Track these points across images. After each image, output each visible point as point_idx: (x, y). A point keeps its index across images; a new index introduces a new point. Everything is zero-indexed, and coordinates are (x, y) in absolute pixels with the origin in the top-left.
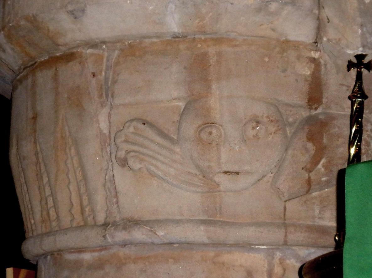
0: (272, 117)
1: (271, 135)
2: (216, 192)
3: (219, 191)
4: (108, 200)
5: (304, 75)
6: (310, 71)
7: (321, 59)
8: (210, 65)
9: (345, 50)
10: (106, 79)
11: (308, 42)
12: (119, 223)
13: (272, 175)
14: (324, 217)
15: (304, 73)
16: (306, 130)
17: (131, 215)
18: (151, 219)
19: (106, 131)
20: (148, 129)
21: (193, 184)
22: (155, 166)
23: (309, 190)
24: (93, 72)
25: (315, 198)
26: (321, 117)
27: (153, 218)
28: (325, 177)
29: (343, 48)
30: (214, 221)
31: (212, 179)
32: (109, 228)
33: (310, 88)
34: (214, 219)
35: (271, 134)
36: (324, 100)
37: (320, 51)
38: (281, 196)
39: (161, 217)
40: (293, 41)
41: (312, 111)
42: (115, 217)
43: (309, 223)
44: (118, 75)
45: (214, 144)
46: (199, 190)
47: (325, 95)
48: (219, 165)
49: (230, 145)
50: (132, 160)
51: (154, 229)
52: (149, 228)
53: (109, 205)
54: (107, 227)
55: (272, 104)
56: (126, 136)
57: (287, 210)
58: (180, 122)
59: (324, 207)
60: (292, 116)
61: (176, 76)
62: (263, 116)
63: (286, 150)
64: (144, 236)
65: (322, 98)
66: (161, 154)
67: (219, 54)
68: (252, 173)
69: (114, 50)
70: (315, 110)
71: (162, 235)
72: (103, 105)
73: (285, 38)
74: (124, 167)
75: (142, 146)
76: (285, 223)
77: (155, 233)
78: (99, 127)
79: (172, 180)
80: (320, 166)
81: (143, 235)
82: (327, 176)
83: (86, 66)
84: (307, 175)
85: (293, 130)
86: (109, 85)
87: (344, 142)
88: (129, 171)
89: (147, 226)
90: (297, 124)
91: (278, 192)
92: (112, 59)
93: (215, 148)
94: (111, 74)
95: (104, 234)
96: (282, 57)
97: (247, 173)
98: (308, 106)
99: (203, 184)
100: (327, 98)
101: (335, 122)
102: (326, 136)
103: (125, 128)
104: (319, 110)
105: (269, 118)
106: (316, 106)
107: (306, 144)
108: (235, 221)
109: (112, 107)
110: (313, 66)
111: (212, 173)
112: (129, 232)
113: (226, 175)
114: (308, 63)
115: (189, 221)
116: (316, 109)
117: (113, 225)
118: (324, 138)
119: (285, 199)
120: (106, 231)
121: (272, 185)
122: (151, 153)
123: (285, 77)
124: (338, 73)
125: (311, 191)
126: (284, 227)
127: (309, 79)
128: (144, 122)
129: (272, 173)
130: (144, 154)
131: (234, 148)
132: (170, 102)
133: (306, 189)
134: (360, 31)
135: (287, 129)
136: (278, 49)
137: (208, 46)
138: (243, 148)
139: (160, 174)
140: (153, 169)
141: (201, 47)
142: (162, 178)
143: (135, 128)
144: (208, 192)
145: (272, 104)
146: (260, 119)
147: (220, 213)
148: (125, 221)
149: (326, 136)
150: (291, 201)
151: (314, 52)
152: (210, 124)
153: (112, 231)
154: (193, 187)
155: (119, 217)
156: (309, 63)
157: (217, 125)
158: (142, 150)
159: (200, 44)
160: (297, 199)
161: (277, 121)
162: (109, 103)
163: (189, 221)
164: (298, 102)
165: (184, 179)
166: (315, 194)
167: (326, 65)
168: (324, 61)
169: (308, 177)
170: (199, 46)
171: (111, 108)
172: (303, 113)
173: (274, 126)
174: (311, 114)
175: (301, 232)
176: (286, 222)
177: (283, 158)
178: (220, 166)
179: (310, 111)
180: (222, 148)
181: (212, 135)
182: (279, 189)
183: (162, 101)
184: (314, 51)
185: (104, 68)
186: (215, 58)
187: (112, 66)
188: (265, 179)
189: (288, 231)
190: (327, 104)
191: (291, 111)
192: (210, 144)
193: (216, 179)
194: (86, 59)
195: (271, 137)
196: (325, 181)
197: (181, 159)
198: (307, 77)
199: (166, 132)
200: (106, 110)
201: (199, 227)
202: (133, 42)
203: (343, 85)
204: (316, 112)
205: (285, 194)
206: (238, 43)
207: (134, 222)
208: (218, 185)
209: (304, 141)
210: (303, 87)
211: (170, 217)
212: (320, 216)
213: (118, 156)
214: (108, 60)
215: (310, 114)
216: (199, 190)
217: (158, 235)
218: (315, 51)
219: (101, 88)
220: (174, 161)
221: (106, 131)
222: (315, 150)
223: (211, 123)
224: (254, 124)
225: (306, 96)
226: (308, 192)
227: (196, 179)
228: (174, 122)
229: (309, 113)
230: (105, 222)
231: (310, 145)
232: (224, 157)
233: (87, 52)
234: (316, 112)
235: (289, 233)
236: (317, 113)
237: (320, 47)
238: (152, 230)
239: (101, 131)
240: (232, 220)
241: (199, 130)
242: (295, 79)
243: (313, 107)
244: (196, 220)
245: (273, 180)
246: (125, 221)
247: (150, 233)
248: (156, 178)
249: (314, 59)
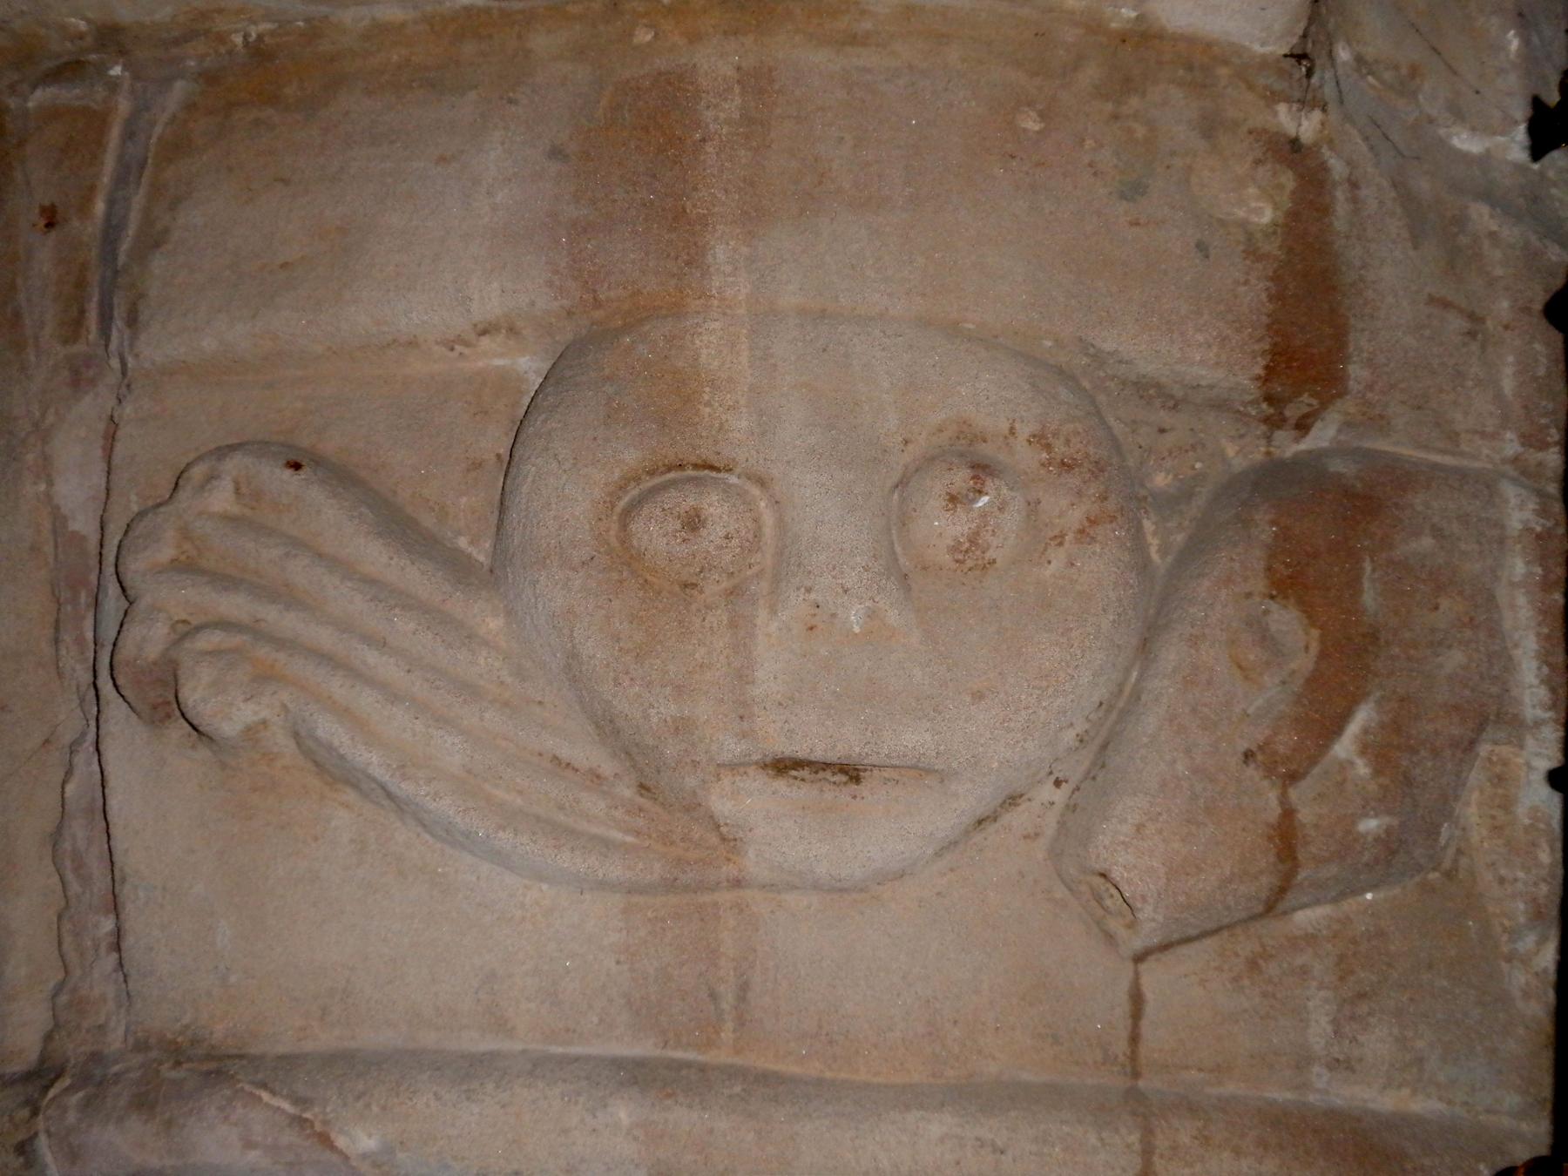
0: (1068, 442)
1: (1061, 544)
2: (715, 887)
3: (737, 883)
4: (67, 926)
5: (1243, 224)
6: (1276, 207)
7: (1331, 149)
8: (703, 140)
9: (1442, 132)
10: (111, 232)
11: (1258, 49)
12: (116, 1068)
13: (1060, 796)
14: (1361, 1060)
15: (1240, 213)
16: (1265, 532)
17: (186, 1020)
18: (308, 1046)
19: (83, 524)
20: (316, 494)
21: (572, 833)
22: (344, 713)
23: (1282, 891)
24: (47, 203)
25: (1311, 939)
26: (1337, 466)
27: (325, 1039)
28: (1376, 816)
29: (1431, 121)
30: (703, 1069)
31: (692, 807)
32: (54, 1099)
33: (1278, 297)
34: (701, 1058)
35: (1060, 539)
36: (1357, 373)
37: (1324, 110)
38: (1114, 925)
39: (371, 1038)
40: (1177, 38)
41: (1281, 436)
42: (101, 1028)
43: (1280, 1095)
44: (173, 206)
45: (713, 587)
46: (615, 870)
47: (1360, 342)
48: (744, 711)
49: (813, 596)
50: (206, 673)
51: (316, 1110)
52: (286, 1106)
53: (72, 957)
54: (47, 1088)
55: (1065, 375)
56: (185, 534)
57: (1150, 1009)
58: (510, 462)
59: (1362, 996)
60: (1168, 463)
61: (499, 198)
62: (1012, 431)
63: (1146, 648)
64: (253, 1156)
65: (1346, 360)
66: (382, 645)
67: (757, 82)
68: (943, 776)
69: (168, 81)
70: (1294, 433)
71: (364, 1156)
72: (79, 377)
73: (1133, 14)
74: (162, 721)
75: (285, 596)
76: (1133, 1096)
77: (325, 1140)
78: (49, 497)
79: (445, 806)
80: (1344, 747)
81: (249, 1145)
82: (1389, 812)
83: (18, 175)
84: (1272, 796)
85: (1179, 538)
86: (122, 259)
87: (1466, 620)
88: (193, 747)
89: (273, 1093)
90: (1201, 500)
91: (1099, 900)
92: (153, 124)
93: (719, 617)
94: (138, 200)
95: (21, 1136)
96: (1116, 117)
97: (919, 771)
98: (1264, 406)
99: (638, 833)
100: (1370, 363)
101: (1418, 500)
102: (1374, 570)
103: (183, 495)
104: (1323, 435)
105: (1048, 447)
106: (1306, 401)
107: (1266, 612)
108: (828, 1075)
109: (126, 381)
110: (1288, 180)
111: (695, 764)
112: (169, 1124)
113: (781, 785)
114: (1258, 162)
115: (541, 1067)
116: (1303, 426)
117: (84, 1079)
118: (1366, 585)
119: (1138, 944)
120: (35, 1113)
121: (1055, 854)
122: (325, 637)
123: (1136, 223)
124: (1416, 241)
125: (1290, 899)
126: (1134, 1114)
127: (1272, 247)
128: (293, 457)
129: (1058, 783)
130: (280, 643)
131: (834, 615)
132: (458, 348)
133: (1267, 881)
134: (1514, 44)
135: (1148, 526)
136: (1091, 74)
137: (695, 38)
138: (893, 617)
139: (372, 761)
140: (328, 729)
141: (649, 44)
142: (389, 795)
143: (244, 490)
144: (670, 886)
145: (1065, 375)
146: (986, 450)
147: (741, 1022)
148: (154, 1054)
149: (1376, 575)
150: (1168, 957)
151: (1290, 109)
152: (690, 472)
153: (72, 1117)
154: (573, 849)
155: (121, 1031)
156: (1269, 166)
157: (733, 479)
158: (271, 614)
159: (649, 26)
160: (1208, 942)
161: (1099, 468)
162: (115, 363)
163: (541, 1067)
164: (1206, 375)
165: (519, 801)
166: (1308, 918)
167: (1354, 185)
168: (1348, 163)
169: (1279, 811)
170: (644, 36)
171: (124, 389)
172: (1231, 451)
173: (1079, 494)
174: (1277, 452)
175: (1238, 1153)
176: (1141, 1084)
177: (1127, 690)
178: (745, 725)
179: (1269, 439)
180: (762, 615)
181: (704, 532)
182: (1103, 875)
183: (412, 343)
184: (1288, 100)
185: (106, 180)
186: (733, 106)
187: (150, 161)
188: (1018, 819)
189: (1161, 1143)
190: (1369, 395)
191: (1162, 431)
192: (686, 586)
193: (721, 804)
194: (21, 144)
195: (1058, 557)
196: (1377, 839)
197: (509, 680)
198: (1259, 235)
199: (428, 521)
200: (90, 407)
201: (605, 1106)
202: (272, 33)
203: (1446, 305)
204: (1306, 445)
205: (1146, 912)
206: (867, 25)
207: (206, 1067)
208: (731, 843)
209: (1249, 595)
210: (1242, 289)
211: (428, 1039)
212: (1336, 1051)
213: (127, 650)
214: (129, 135)
215: (1268, 453)
216: (615, 870)
217: (340, 1152)
218: (1295, 107)
219: (81, 284)
220: (470, 691)
221: (83, 524)
222: (1315, 648)
223: (696, 466)
224: (961, 478)
225: (1259, 340)
226: (1273, 905)
227: (595, 804)
228: (477, 465)
229: (1263, 449)
230: (43, 1059)
231: (1285, 620)
232: (770, 676)
233: (30, 105)
234: (1306, 445)
235: (1162, 1156)
236: (1309, 452)
237: (1321, 87)
238: (307, 1115)
239: (59, 520)
240: (814, 1069)
241: (622, 504)
242: (1193, 244)
243: (1292, 412)
244: (587, 1059)
245: (1062, 824)
246: (154, 1054)
247: (289, 1137)
248: (350, 796)
249: (1295, 144)
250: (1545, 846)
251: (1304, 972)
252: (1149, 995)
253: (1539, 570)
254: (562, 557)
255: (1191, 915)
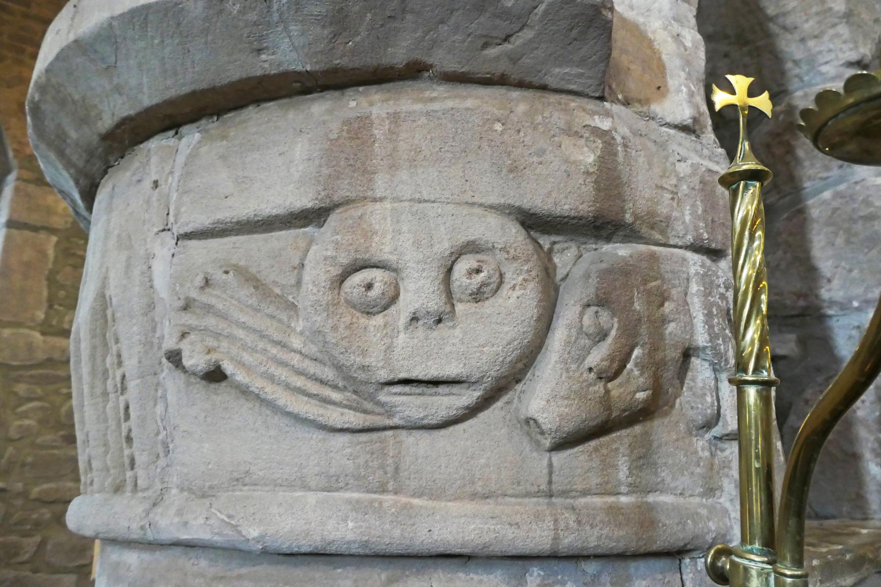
7: (616, 132)
67: (395, 118)
137: (371, 104)
169: (604, 392)
211: (368, 263)
250: (709, 395)
251: (617, 449)
252: (555, 464)
253: (703, 289)
254: (255, 459)
255: (582, 374)
